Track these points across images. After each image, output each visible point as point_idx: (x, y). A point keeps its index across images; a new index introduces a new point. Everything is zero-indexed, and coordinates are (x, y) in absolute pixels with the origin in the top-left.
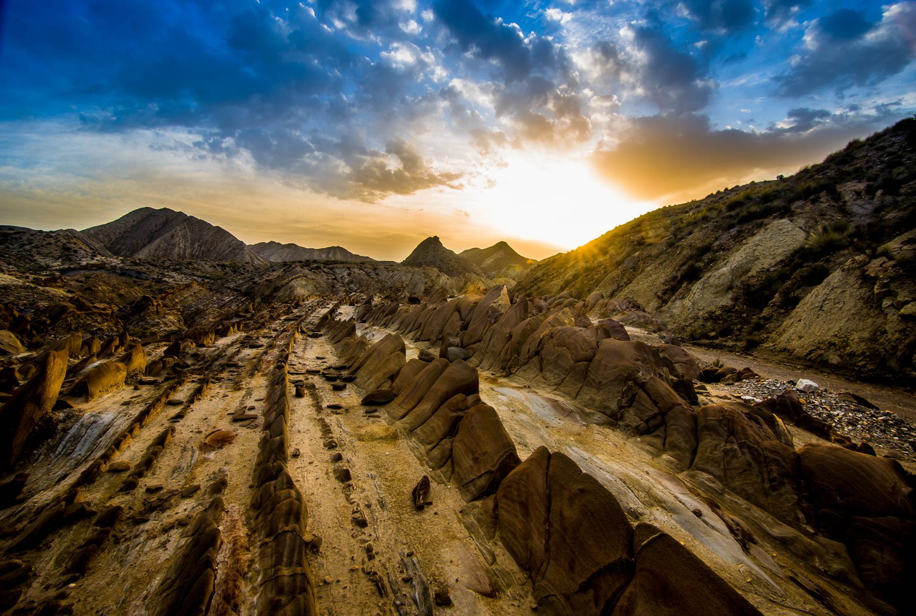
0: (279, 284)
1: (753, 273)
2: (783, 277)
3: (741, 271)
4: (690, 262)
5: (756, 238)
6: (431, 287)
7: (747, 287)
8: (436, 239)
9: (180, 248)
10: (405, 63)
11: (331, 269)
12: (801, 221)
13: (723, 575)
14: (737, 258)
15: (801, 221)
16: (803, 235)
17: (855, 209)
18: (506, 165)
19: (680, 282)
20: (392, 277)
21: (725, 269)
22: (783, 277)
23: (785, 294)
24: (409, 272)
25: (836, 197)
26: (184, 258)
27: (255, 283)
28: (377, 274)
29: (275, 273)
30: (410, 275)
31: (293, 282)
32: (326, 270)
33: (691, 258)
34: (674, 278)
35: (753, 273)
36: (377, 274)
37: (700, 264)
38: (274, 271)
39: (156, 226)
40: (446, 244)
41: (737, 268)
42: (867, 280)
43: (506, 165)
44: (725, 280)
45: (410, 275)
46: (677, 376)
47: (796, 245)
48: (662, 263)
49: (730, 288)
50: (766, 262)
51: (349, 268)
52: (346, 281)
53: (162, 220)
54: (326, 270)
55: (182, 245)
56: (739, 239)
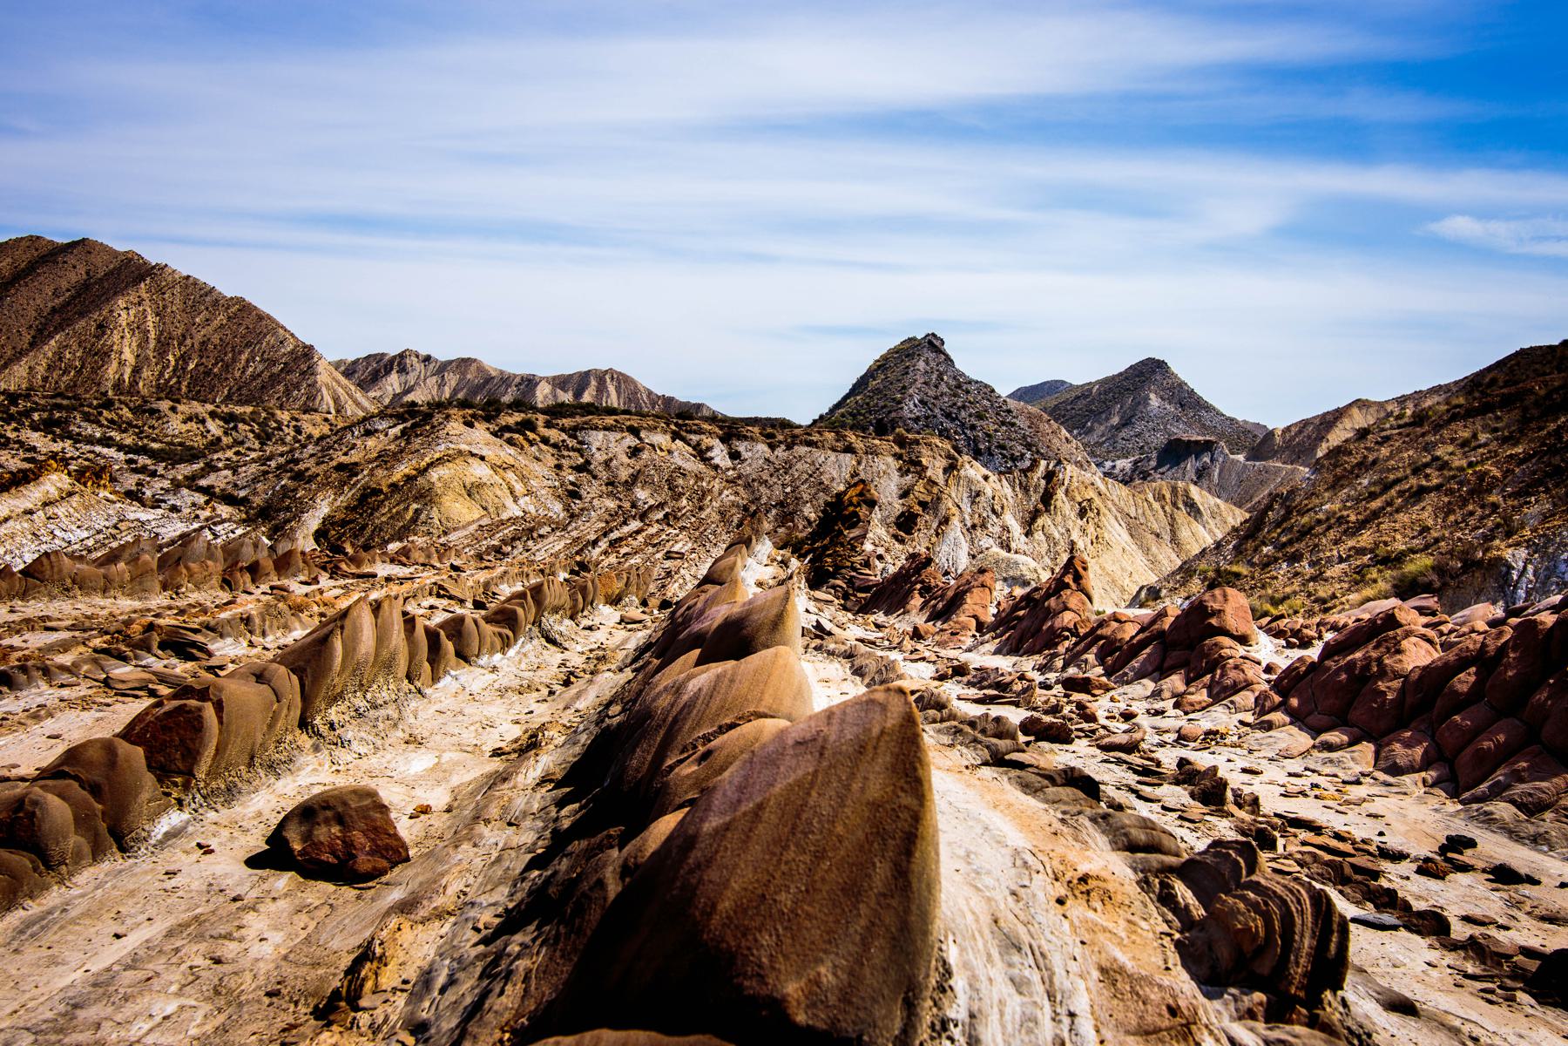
0: (383, 479)
8: (933, 344)
9: (122, 363)
11: (572, 432)
18: (212, 851)
20: (788, 466)
26: (132, 389)
27: (299, 476)
29: (371, 442)
31: (434, 475)
32: (554, 435)
38: (368, 433)
39: (56, 294)
40: (970, 361)
43: (212, 851)
46: (1143, 644)
51: (634, 431)
52: (624, 474)
53: (73, 278)
54: (554, 435)
55: (129, 356)
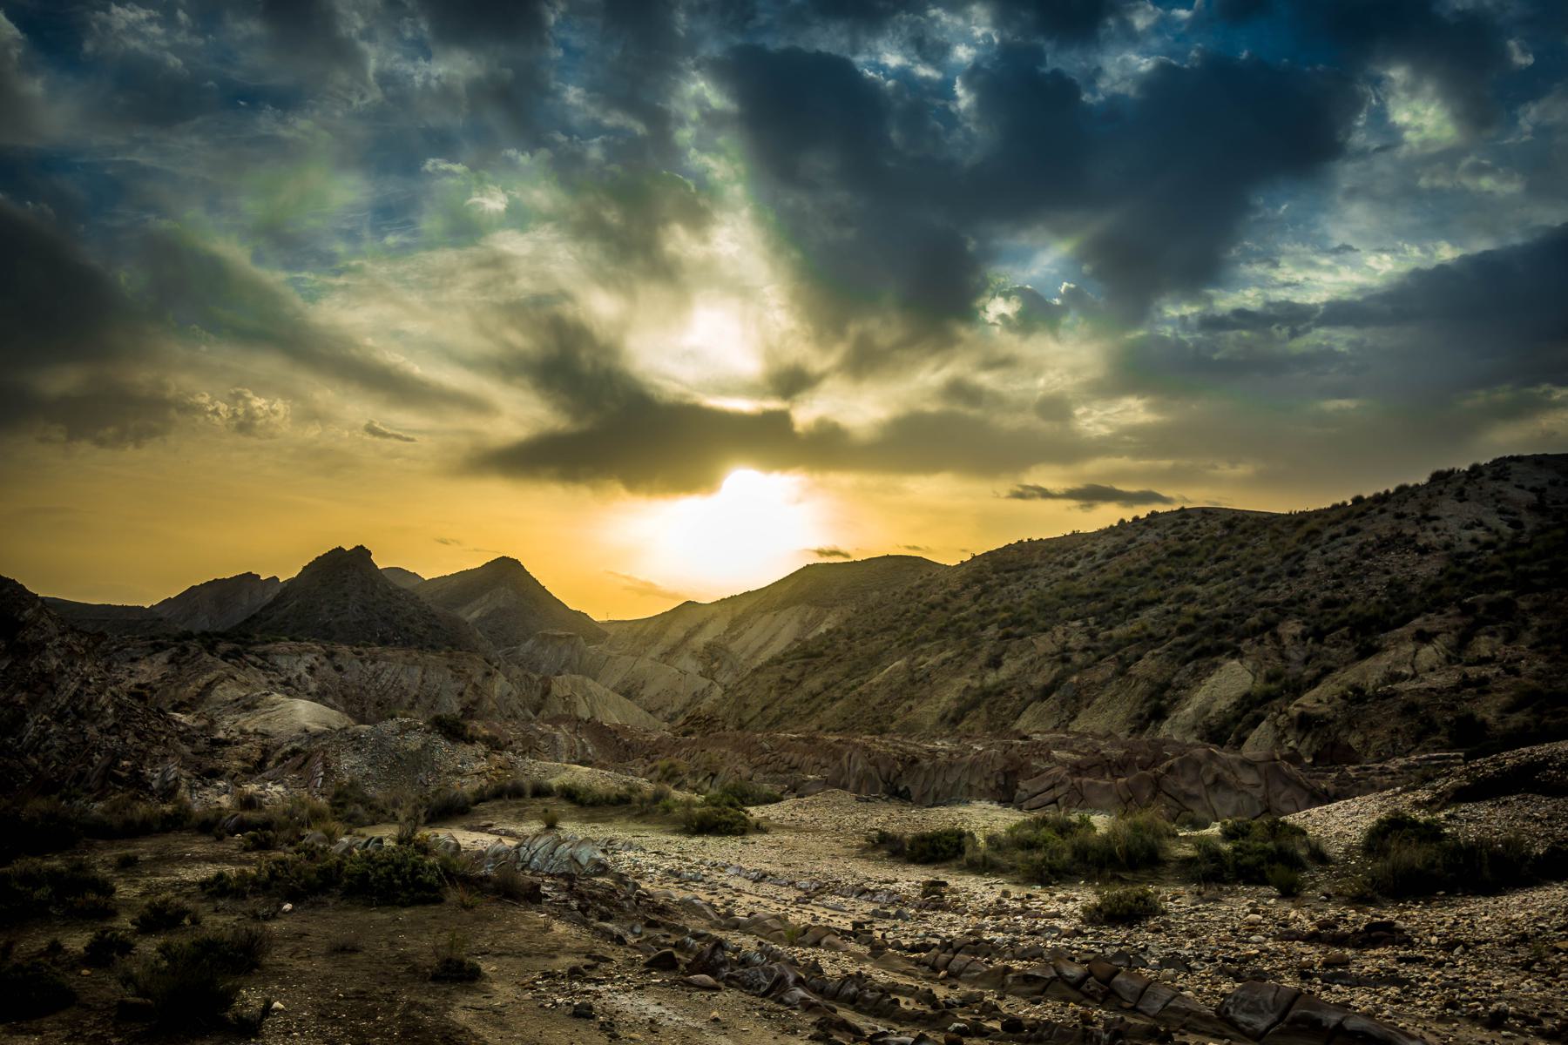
1: (1212, 714)
2: (1237, 720)
3: (1203, 711)
4: (1154, 701)
5: (1213, 679)
6: (474, 703)
7: (1208, 726)
8: (362, 553)
10: (491, 197)
12: (1249, 664)
13: (1346, 297)
14: (1198, 698)
15: (1249, 664)
16: (1250, 678)
17: (1292, 655)
19: (1148, 721)
21: (1189, 710)
22: (1237, 720)
23: (1238, 734)
24: (415, 663)
25: (1277, 638)
28: (339, 669)
30: (417, 671)
33: (1151, 695)
34: (1140, 716)
35: (1212, 714)
36: (339, 669)
37: (1164, 703)
41: (1199, 709)
42: (1277, 727)
44: (1190, 721)
45: (417, 671)
47: (1246, 688)
48: (1114, 696)
49: (1195, 728)
50: (1222, 704)
56: (1198, 676)
